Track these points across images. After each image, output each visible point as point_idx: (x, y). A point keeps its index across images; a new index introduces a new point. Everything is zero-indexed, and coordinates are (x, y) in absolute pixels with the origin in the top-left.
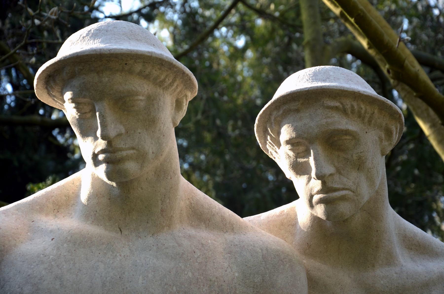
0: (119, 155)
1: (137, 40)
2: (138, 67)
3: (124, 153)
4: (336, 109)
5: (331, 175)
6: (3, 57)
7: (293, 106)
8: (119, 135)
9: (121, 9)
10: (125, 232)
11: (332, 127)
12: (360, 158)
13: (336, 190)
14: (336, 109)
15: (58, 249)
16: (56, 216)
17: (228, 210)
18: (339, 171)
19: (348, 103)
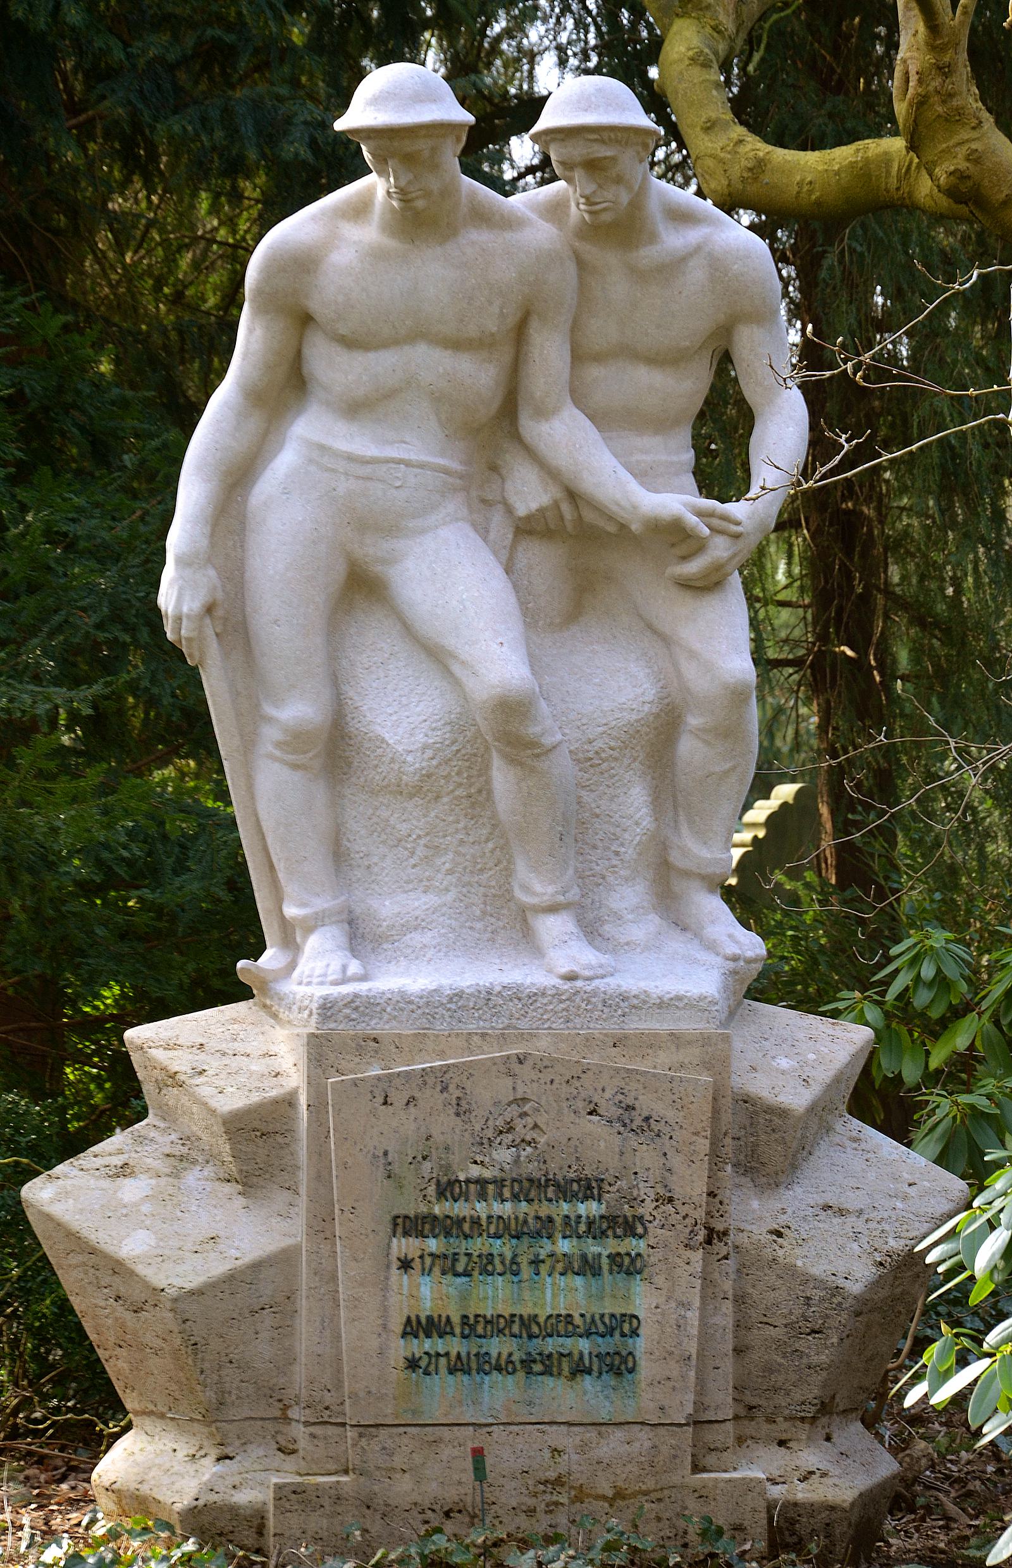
0: (409, 196)
1: (421, 101)
2: (423, 132)
3: (414, 195)
4: (596, 140)
5: (594, 192)
6: (280, 6)
7: (559, 136)
8: (409, 182)
9: (408, 630)
10: (417, 243)
11: (592, 156)
12: (618, 175)
13: (597, 204)
14: (596, 140)
15: (362, 262)
16: (356, 222)
17: (259, 890)
18: (600, 186)
19: (605, 135)
